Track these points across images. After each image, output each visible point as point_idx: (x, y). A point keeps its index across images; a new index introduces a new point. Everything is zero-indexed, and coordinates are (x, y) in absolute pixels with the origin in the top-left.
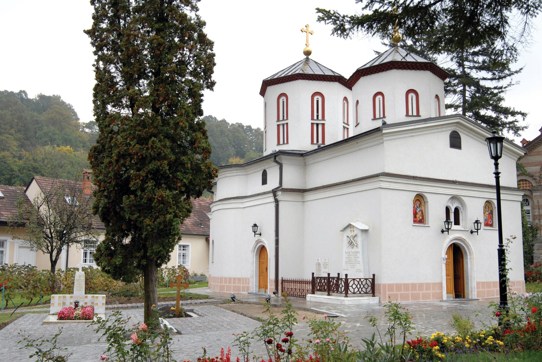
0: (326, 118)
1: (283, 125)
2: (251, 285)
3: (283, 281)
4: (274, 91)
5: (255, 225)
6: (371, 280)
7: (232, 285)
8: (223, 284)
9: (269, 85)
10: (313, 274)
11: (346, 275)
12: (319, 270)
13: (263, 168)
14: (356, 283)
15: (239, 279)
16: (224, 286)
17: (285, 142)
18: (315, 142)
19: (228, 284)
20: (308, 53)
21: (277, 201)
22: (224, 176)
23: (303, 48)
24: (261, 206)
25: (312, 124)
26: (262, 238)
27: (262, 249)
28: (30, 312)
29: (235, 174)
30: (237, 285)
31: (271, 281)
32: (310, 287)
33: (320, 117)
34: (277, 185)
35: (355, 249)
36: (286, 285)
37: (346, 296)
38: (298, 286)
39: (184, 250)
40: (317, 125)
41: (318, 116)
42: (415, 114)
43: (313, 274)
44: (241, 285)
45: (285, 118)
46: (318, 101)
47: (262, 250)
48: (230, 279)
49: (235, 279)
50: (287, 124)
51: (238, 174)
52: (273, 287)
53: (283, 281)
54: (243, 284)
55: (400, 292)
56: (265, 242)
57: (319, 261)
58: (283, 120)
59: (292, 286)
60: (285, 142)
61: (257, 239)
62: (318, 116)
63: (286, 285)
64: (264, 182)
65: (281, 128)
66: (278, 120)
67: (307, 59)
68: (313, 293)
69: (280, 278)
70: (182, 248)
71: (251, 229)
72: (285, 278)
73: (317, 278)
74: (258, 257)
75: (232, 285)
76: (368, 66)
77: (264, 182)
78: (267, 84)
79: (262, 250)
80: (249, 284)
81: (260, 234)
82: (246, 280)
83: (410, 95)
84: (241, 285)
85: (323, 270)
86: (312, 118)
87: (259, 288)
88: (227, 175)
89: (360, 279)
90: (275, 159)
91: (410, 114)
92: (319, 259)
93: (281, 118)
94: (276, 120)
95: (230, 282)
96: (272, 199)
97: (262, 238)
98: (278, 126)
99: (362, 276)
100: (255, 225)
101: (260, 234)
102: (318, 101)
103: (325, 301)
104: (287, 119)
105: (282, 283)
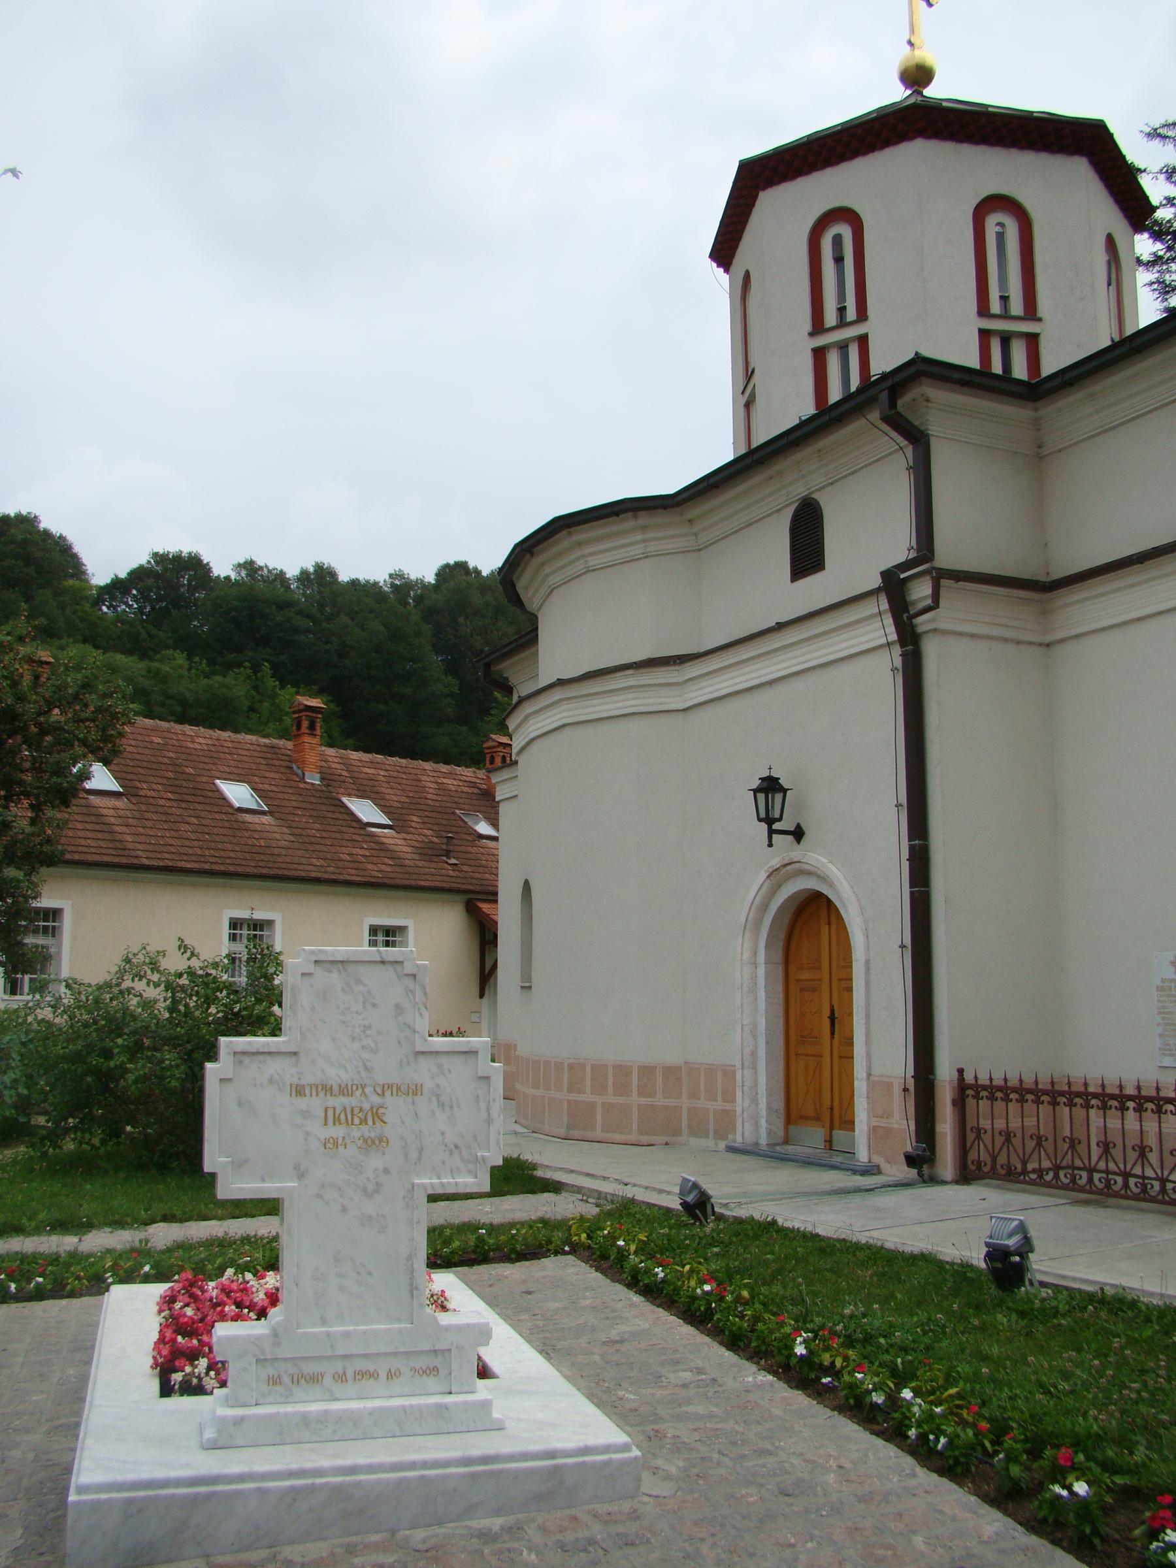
0: (1043, 308)
1: (843, 347)
2: (741, 1102)
3: (964, 1090)
4: (787, 211)
5: (770, 786)
7: (635, 1099)
8: (586, 1097)
9: (764, 189)
13: (798, 491)
15: (672, 1073)
16: (592, 1106)
18: (995, 307)
19: (610, 1098)
21: (909, 640)
22: (579, 567)
23: (897, 57)
24: (799, 684)
26: (812, 855)
29: (636, 551)
30: (659, 1100)
31: (877, 1087)
33: (1016, 308)
34: (897, 546)
36: (983, 1114)
38: (1036, 1118)
39: (387, 944)
44: (685, 1102)
45: (851, 314)
46: (1000, 237)
47: (807, 926)
48: (622, 1070)
49: (647, 1070)
50: (863, 340)
51: (653, 547)
52: (902, 1122)
53: (964, 1090)
54: (694, 1095)
56: (834, 872)
58: (842, 324)
59: (1012, 1117)
61: (775, 862)
62: (1004, 299)
63: (983, 1114)
64: (807, 556)
66: (818, 327)
69: (945, 1072)
70: (381, 938)
71: (746, 805)
72: (981, 1071)
74: (779, 956)
75: (635, 1099)
77: (807, 556)
78: (758, 176)
79: (807, 926)
80: (730, 1097)
81: (798, 834)
82: (720, 1079)
84: (685, 1102)
86: (983, 310)
87: (788, 1121)
88: (593, 561)
90: (893, 404)
93: (831, 318)
94: (808, 327)
95: (622, 1088)
96: (883, 630)
97: (812, 855)
98: (819, 354)
100: (770, 786)
101: (798, 834)
102: (1000, 237)
104: (862, 315)
105: (960, 1103)
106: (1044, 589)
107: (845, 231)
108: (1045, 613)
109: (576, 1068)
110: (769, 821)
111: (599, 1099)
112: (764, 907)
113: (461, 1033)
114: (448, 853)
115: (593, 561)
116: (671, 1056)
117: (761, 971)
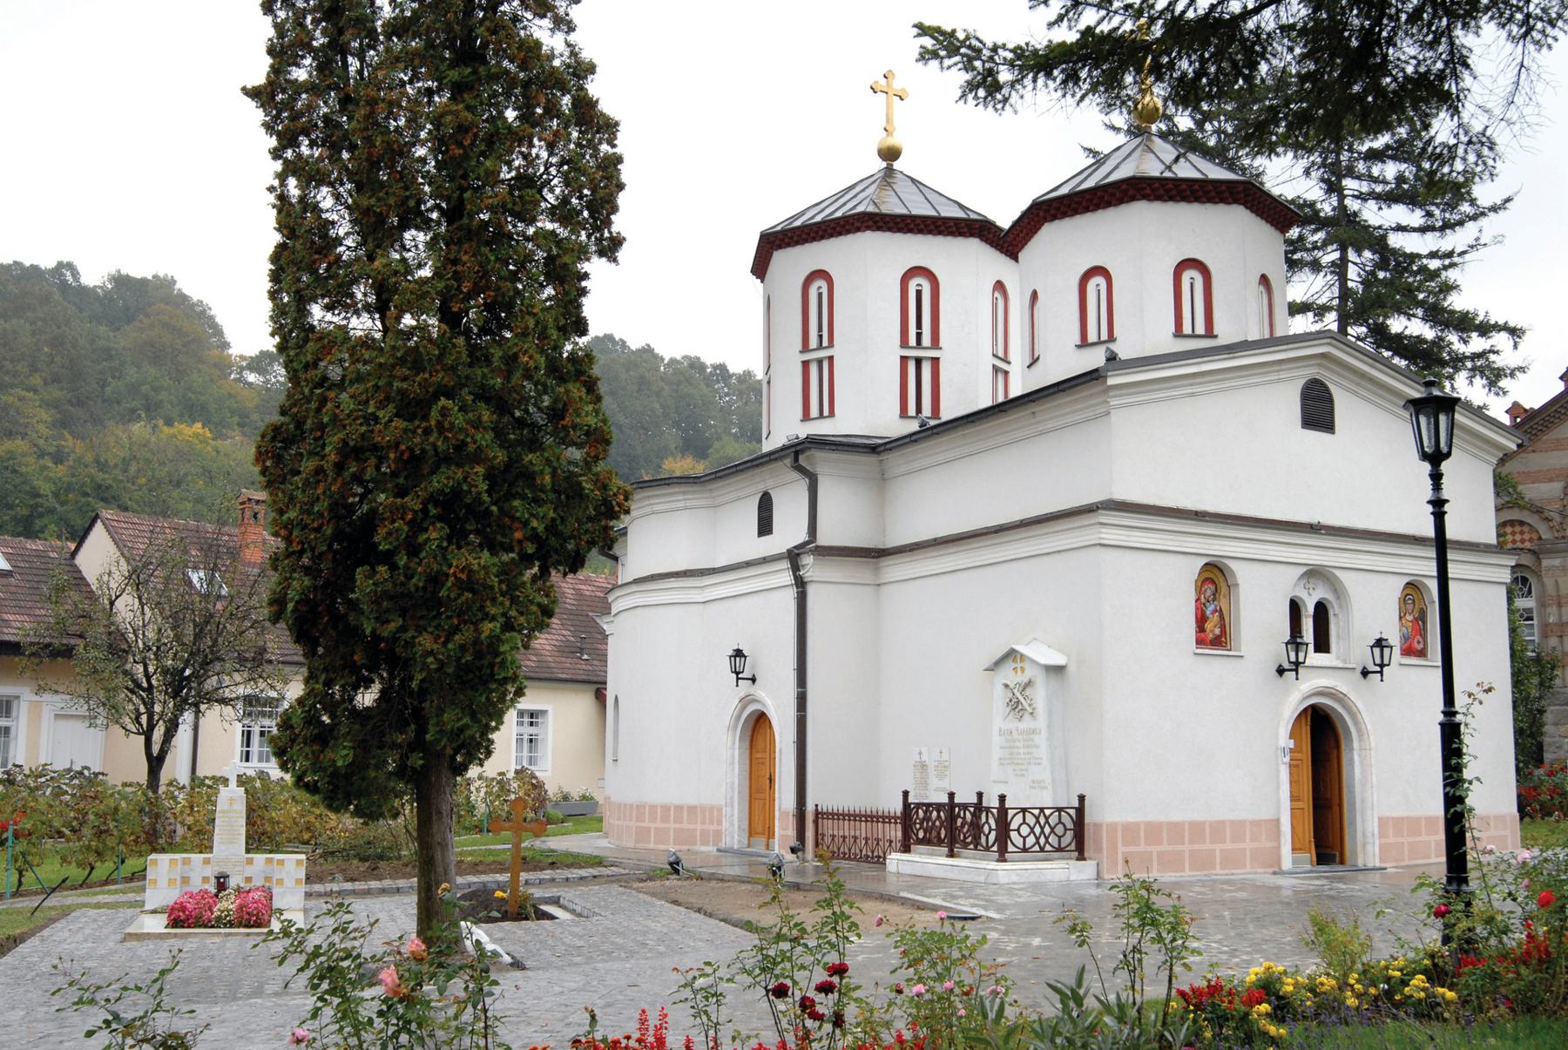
0: (942, 343)
1: (820, 362)
2: (725, 825)
3: (818, 814)
4: (793, 263)
5: (739, 653)
6: (1072, 812)
9: (780, 247)
10: (906, 794)
11: (1002, 798)
12: (924, 784)
13: (761, 487)
14: (1031, 820)
15: (692, 809)
16: (648, 830)
17: (826, 412)
18: (912, 411)
19: (659, 825)
20: (890, 154)
21: (801, 584)
22: (648, 510)
23: (877, 139)
25: (904, 359)
26: (759, 691)
27: (759, 723)
28: (86, 905)
30: (685, 826)
31: (784, 814)
32: (896, 832)
33: (926, 340)
34: (801, 536)
35: (1027, 723)
36: (828, 827)
37: (1002, 859)
38: (863, 829)
39: (531, 724)
40: (919, 361)
41: (919, 335)
42: (1200, 329)
43: (906, 794)
44: (699, 827)
45: (825, 343)
46: (919, 293)
48: (666, 808)
49: (679, 808)
50: (831, 359)
52: (791, 832)
53: (818, 814)
54: (703, 823)
55: (1159, 848)
57: (924, 758)
58: (820, 347)
59: (846, 829)
60: (826, 412)
61: (742, 694)
62: (919, 335)
63: (828, 827)
64: (765, 527)
65: (814, 369)
66: (805, 348)
67: (889, 172)
68: (906, 849)
69: (810, 807)
70: (526, 720)
71: (725, 665)
73: (918, 806)
74: (747, 744)
75: (672, 825)
76: (1064, 191)
77: (765, 527)
78: (772, 243)
81: (753, 680)
82: (713, 813)
83: (1187, 276)
84: (699, 827)
85: (934, 782)
86: (904, 343)
87: (750, 835)
88: (656, 508)
89: (1042, 810)
91: (1187, 329)
92: (924, 750)
93: (813, 343)
94: (799, 346)
95: (665, 819)
96: (787, 578)
97: (759, 691)
98: (806, 364)
99: (1046, 799)
100: (739, 653)
101: (753, 680)
102: (919, 293)
103: (939, 873)
105: (816, 822)
106: (876, 555)
107: (823, 284)
108: (877, 569)
109: (640, 807)
110: (737, 673)
111: (653, 825)
112: (739, 717)
113: (817, 845)
114: (581, 650)
115: (656, 508)
116: (691, 800)
117: (737, 753)
